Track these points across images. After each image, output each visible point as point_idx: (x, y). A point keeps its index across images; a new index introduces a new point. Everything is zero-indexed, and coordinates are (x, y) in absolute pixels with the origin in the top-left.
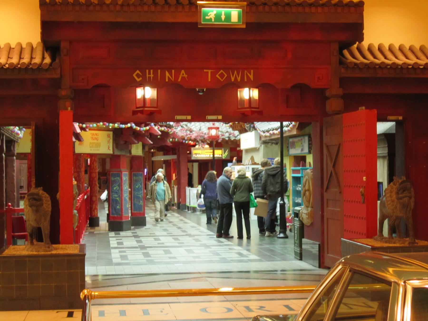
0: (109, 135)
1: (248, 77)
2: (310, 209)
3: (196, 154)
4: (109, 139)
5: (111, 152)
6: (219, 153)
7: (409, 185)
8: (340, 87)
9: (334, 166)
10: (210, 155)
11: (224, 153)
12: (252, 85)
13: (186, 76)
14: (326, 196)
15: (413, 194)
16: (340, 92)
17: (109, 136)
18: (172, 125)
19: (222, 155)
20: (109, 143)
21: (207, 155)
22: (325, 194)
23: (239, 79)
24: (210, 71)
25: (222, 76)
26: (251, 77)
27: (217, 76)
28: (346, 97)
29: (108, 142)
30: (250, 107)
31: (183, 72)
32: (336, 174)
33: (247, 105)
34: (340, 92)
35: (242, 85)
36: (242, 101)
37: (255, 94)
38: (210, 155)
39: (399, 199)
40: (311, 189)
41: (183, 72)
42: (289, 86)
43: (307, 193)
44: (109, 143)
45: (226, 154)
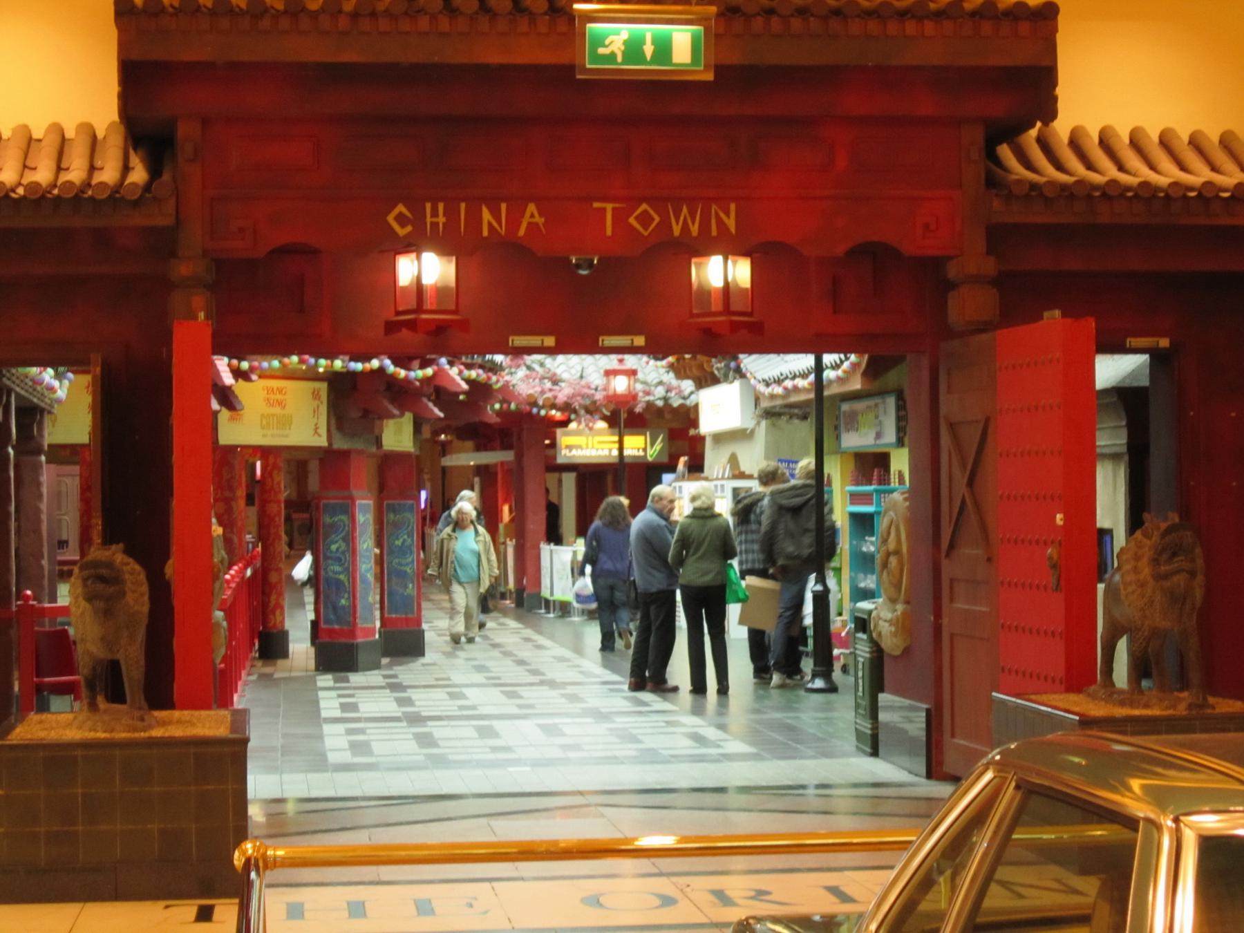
0: (316, 393)
1: (720, 223)
2: (900, 607)
3: (570, 447)
4: (316, 402)
5: (322, 441)
6: (636, 445)
7: (1188, 537)
8: (988, 253)
9: (971, 483)
10: (610, 450)
11: (652, 445)
12: (732, 247)
13: (539, 220)
14: (948, 569)
15: (1200, 563)
16: (989, 266)
17: (316, 395)
18: (502, 363)
19: (645, 450)
20: (316, 416)
21: (603, 450)
22: (945, 563)
23: (695, 229)
24: (609, 207)
25: (645, 219)
26: (731, 223)
27: (632, 220)
28: (1003, 282)
29: (314, 412)
30: (727, 310)
31: (532, 208)
32: (977, 505)
33: (717, 305)
34: (989, 266)
35: (703, 248)
36: (705, 293)
37: (741, 272)
38: (610, 450)
39: (1159, 577)
40: (905, 549)
41: (532, 208)
42: (840, 250)
43: (893, 561)
44: (316, 416)
45: (658, 446)
